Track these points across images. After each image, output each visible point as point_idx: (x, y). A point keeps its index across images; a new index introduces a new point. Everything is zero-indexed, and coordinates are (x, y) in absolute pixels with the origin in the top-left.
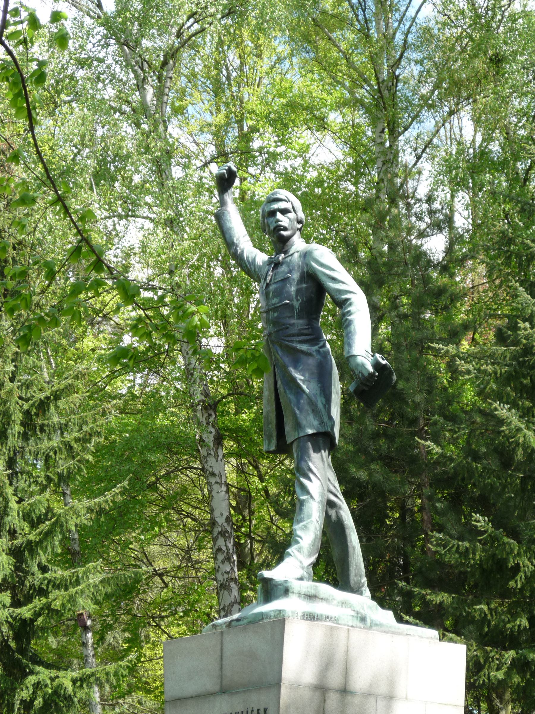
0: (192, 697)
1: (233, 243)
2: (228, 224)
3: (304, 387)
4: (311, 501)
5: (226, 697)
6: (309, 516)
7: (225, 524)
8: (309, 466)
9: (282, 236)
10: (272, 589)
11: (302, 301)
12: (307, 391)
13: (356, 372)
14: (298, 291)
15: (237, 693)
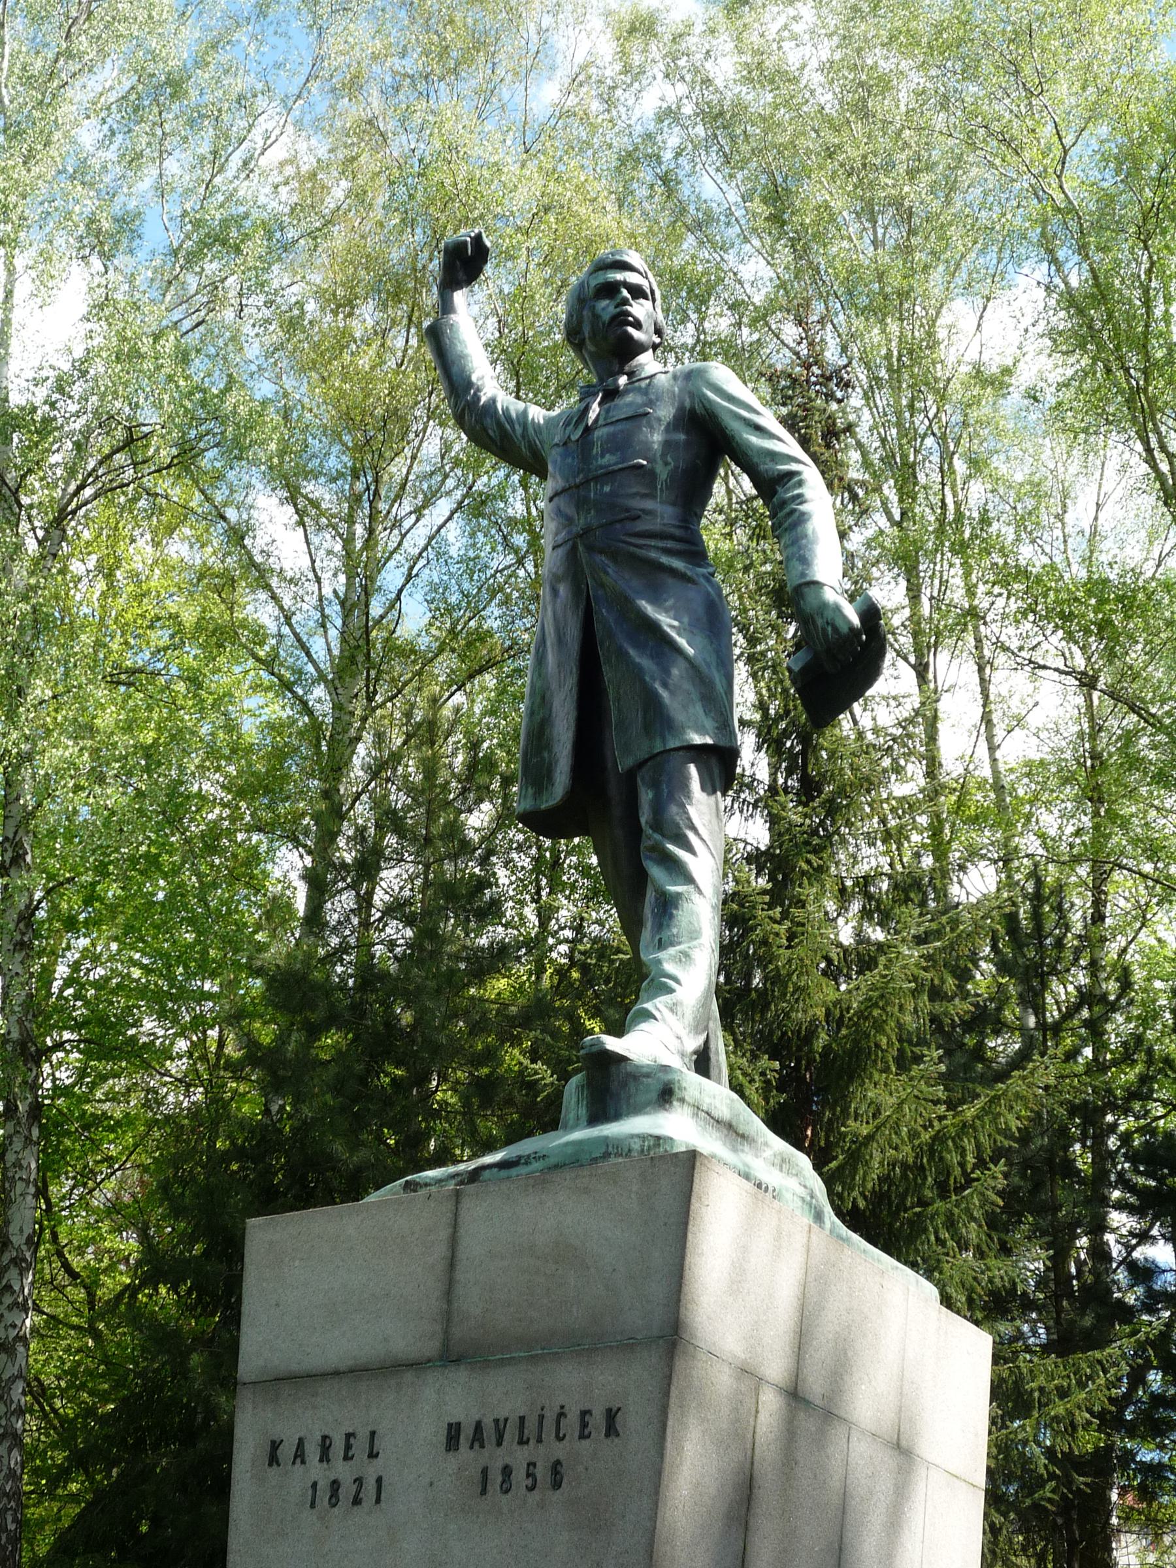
0: (336, 1373)
1: (469, 384)
2: (459, 348)
3: (682, 642)
4: (695, 897)
5: (461, 1375)
6: (694, 934)
7: (24, 1248)
8: (689, 819)
9: (630, 337)
10: (624, 1085)
11: (676, 468)
12: (690, 651)
13: (820, 622)
14: (667, 445)
15: (502, 1363)
